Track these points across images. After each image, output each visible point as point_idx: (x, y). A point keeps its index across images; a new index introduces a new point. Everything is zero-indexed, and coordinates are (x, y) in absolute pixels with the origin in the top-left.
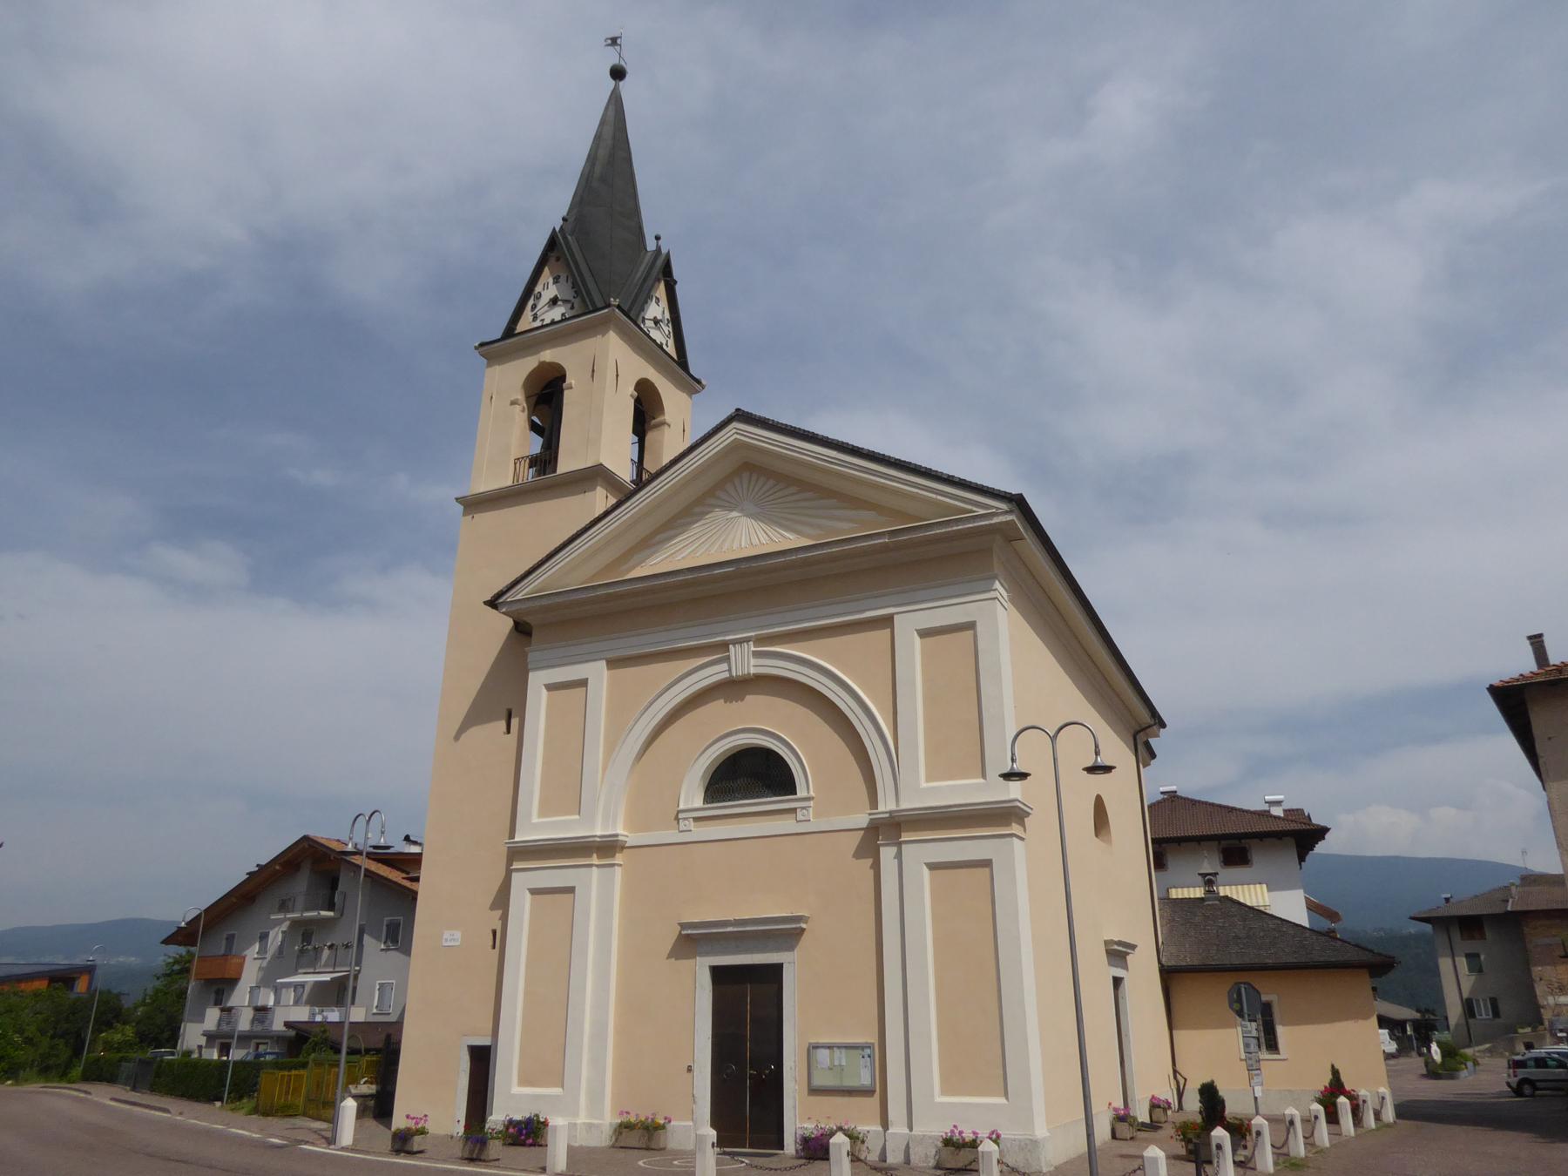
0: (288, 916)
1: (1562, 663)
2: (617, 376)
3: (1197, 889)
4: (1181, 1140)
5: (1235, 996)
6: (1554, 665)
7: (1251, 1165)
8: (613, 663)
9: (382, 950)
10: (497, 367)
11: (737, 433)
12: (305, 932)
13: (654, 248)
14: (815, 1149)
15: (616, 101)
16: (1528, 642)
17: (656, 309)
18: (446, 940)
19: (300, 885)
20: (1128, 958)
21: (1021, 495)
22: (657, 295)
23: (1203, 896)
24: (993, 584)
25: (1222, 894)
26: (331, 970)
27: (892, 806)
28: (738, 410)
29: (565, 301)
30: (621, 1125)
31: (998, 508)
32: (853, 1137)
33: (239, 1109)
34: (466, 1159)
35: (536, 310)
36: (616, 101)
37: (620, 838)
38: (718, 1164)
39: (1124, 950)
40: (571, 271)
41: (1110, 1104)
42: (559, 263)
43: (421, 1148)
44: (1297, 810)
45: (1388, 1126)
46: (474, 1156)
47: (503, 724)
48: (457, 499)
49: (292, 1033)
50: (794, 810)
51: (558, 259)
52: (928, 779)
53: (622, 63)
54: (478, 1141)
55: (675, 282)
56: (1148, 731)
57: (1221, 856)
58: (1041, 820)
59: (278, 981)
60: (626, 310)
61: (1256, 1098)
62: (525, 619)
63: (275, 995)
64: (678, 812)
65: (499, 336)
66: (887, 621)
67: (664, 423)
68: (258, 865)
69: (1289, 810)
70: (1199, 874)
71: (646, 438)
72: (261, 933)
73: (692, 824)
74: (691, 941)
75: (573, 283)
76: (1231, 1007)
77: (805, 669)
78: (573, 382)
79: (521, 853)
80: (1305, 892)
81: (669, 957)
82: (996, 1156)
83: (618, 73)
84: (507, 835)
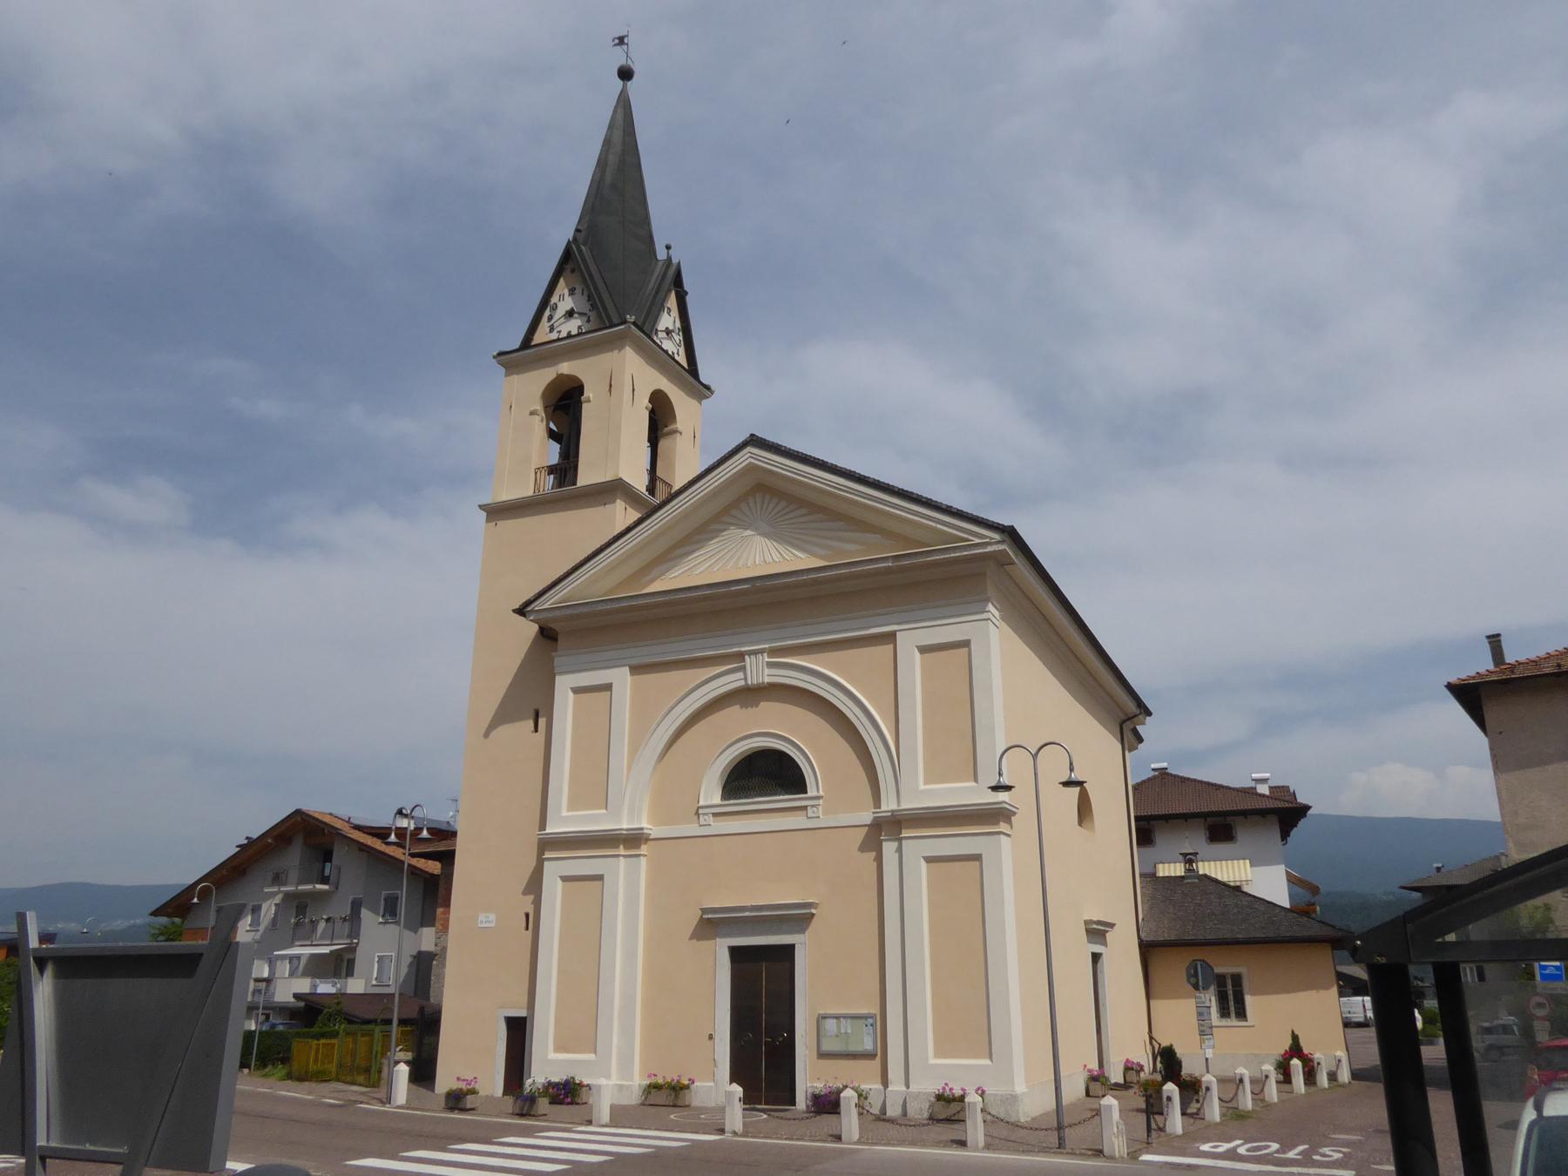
0: (282, 889)
1: (1517, 661)
2: (633, 390)
3: (1178, 864)
4: (1143, 1096)
5: (1192, 971)
6: (1509, 664)
7: (1201, 1116)
8: (636, 669)
9: (381, 923)
10: (515, 376)
11: (750, 457)
12: (299, 905)
13: (665, 258)
14: (827, 1104)
15: (624, 104)
16: (1486, 641)
17: (669, 320)
18: (482, 922)
19: (293, 858)
20: (1107, 935)
21: (1013, 526)
22: (669, 305)
23: (1183, 874)
24: (986, 605)
25: (1201, 872)
26: (328, 942)
27: (894, 806)
28: (752, 435)
29: (581, 314)
30: (650, 1086)
31: (991, 538)
32: (861, 1095)
33: (269, 1075)
34: (517, 1114)
35: (552, 322)
36: (624, 104)
37: (645, 831)
38: (743, 1118)
39: (1103, 928)
40: (588, 287)
41: (1085, 1066)
42: (574, 275)
43: (473, 1106)
44: (1283, 787)
45: (1343, 1086)
46: (525, 1112)
47: (531, 723)
48: (480, 506)
49: (302, 1004)
50: (805, 808)
51: (573, 271)
52: (926, 783)
53: (630, 62)
54: (527, 1099)
55: (686, 293)
56: (1134, 719)
57: (1207, 833)
58: (1024, 821)
59: (275, 953)
60: (639, 324)
61: (1207, 1059)
62: (553, 626)
63: (269, 966)
64: (698, 808)
65: (517, 345)
66: (890, 638)
67: (675, 431)
68: (247, 838)
69: (1276, 787)
70: (1181, 854)
71: (659, 446)
72: (253, 906)
73: (711, 818)
74: (711, 925)
75: (589, 296)
76: (1188, 981)
77: (819, 680)
78: (591, 395)
79: (549, 844)
80: (1286, 866)
81: (690, 939)
82: (980, 1106)
83: (625, 74)
84: (537, 827)
